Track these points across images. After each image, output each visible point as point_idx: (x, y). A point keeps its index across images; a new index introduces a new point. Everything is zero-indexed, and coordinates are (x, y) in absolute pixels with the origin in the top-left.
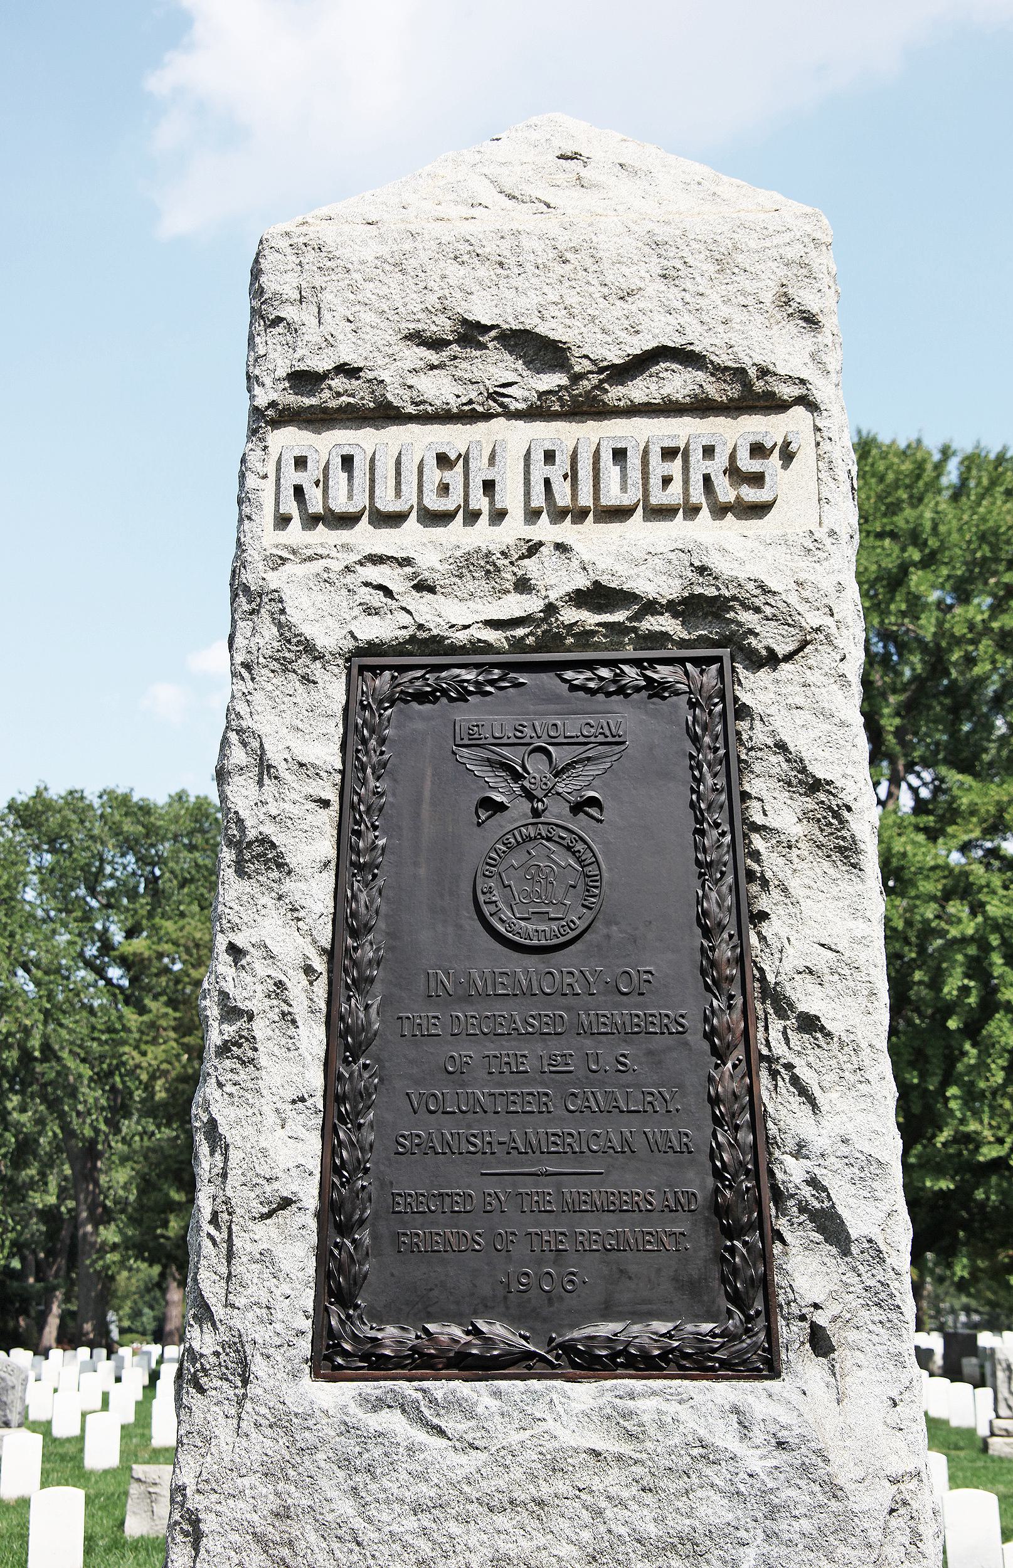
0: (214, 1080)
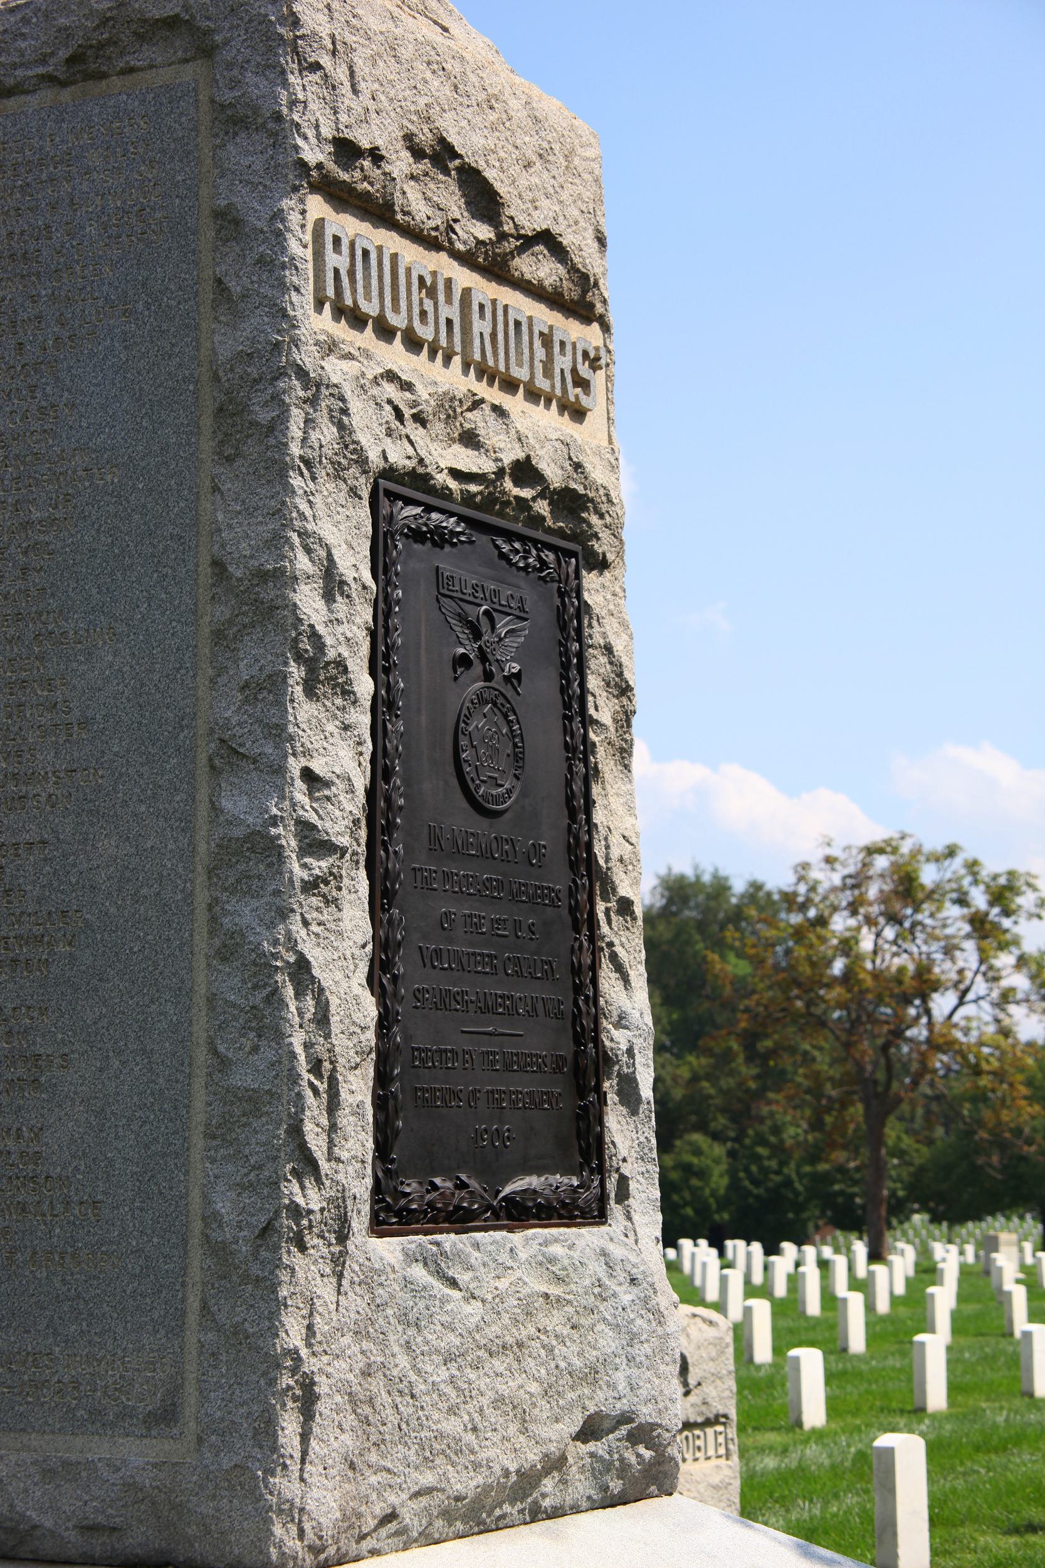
0: (298, 918)
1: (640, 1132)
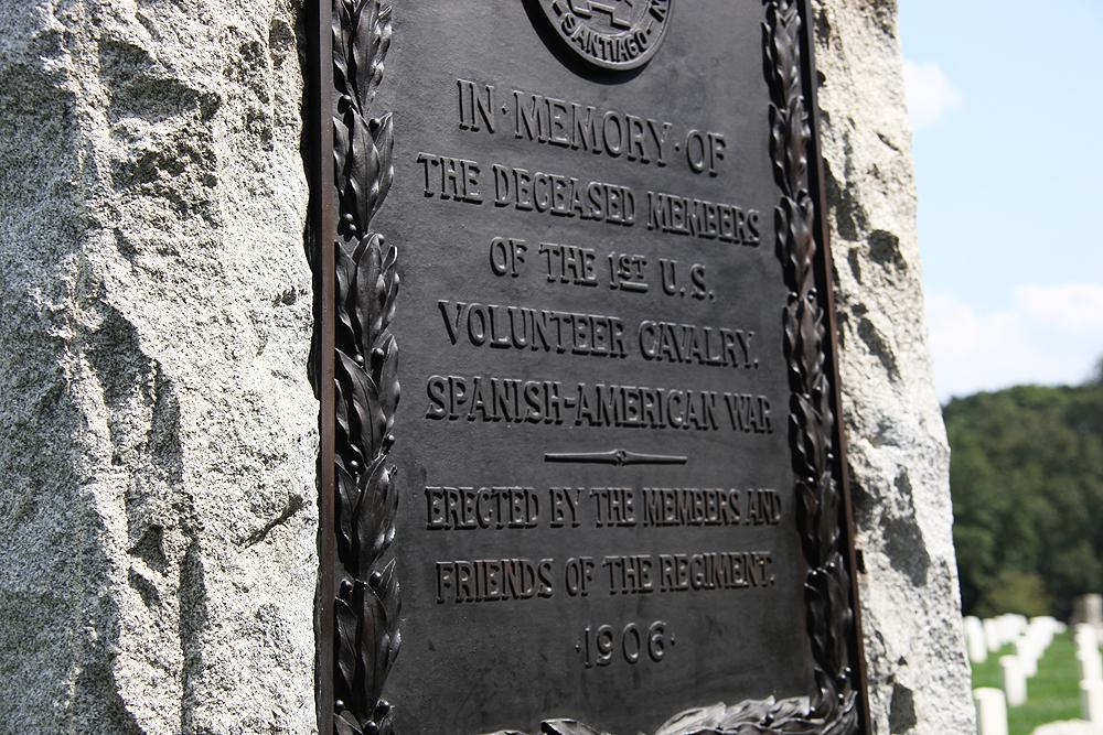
0: (109, 239)
1: (932, 613)
